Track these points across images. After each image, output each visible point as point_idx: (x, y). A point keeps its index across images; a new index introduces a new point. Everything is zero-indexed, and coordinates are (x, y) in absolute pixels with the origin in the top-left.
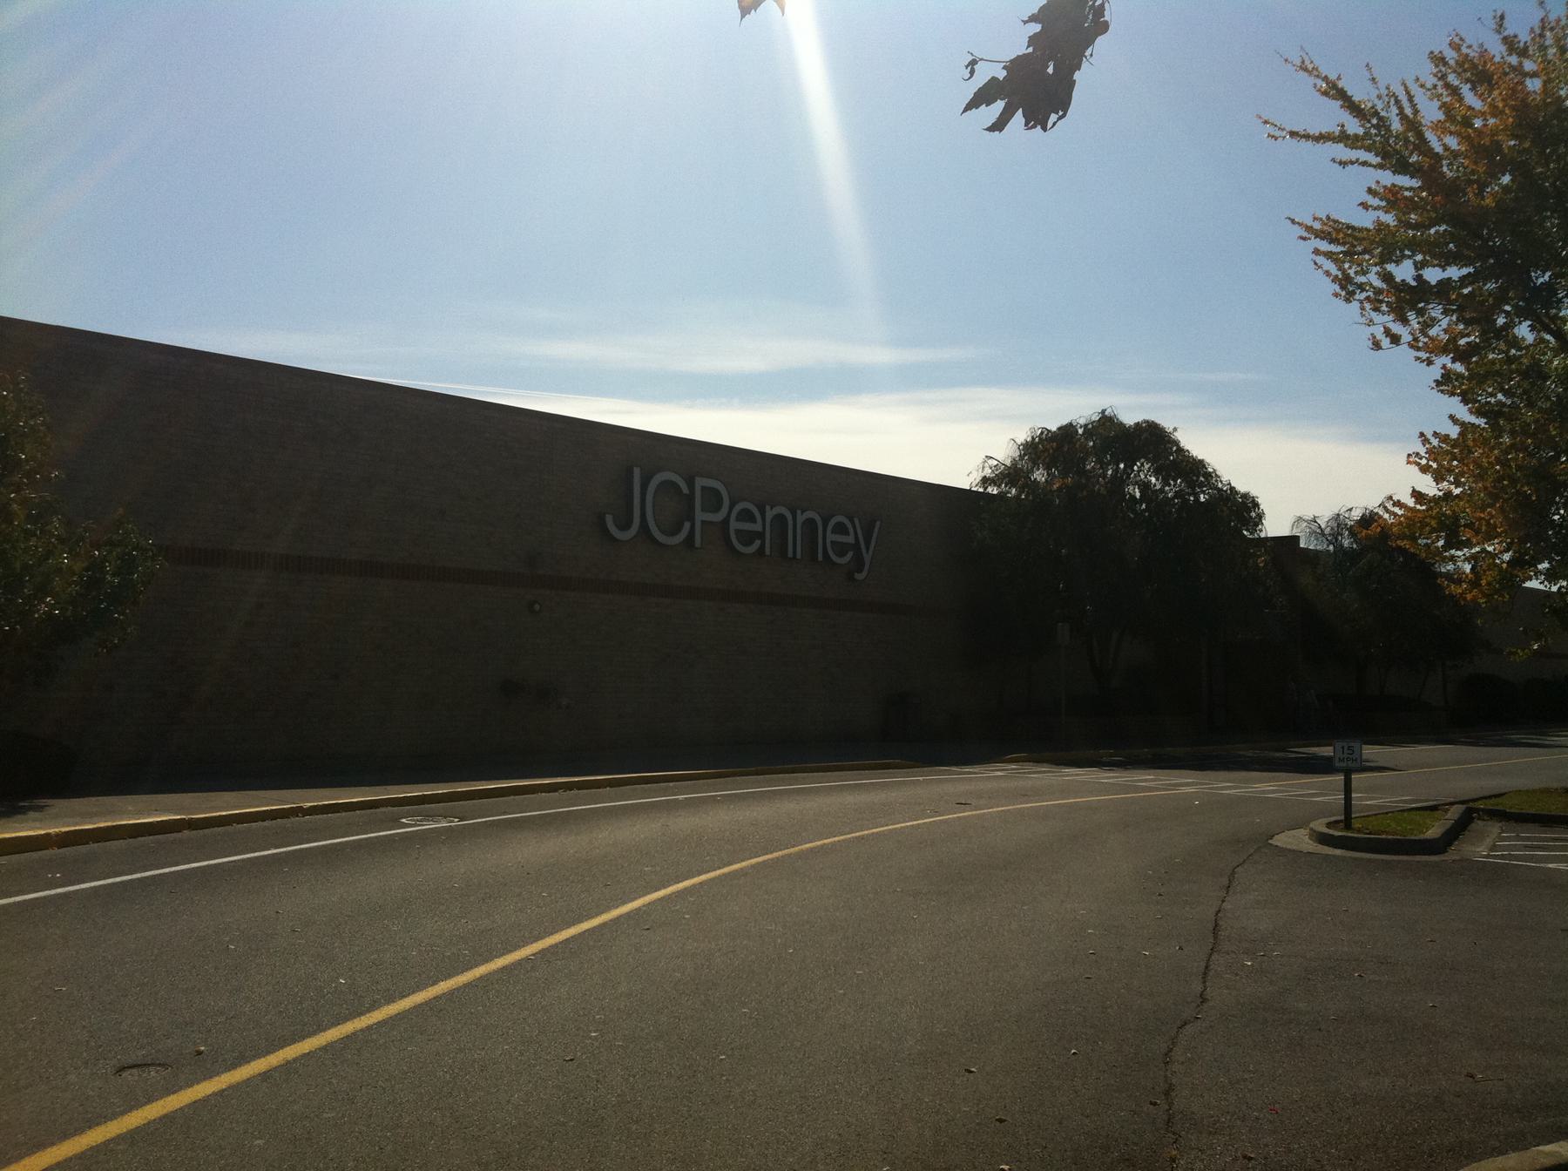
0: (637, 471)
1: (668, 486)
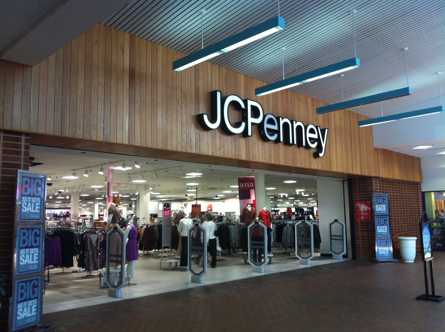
0: (219, 94)
1: (234, 104)
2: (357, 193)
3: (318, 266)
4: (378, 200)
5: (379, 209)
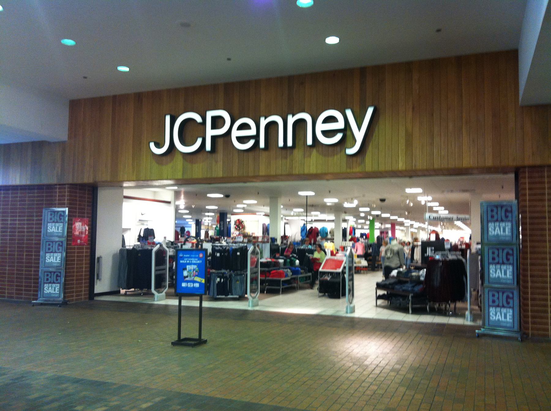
2: (16, 273)
3: (518, 70)
4: (49, 277)
5: (49, 291)
